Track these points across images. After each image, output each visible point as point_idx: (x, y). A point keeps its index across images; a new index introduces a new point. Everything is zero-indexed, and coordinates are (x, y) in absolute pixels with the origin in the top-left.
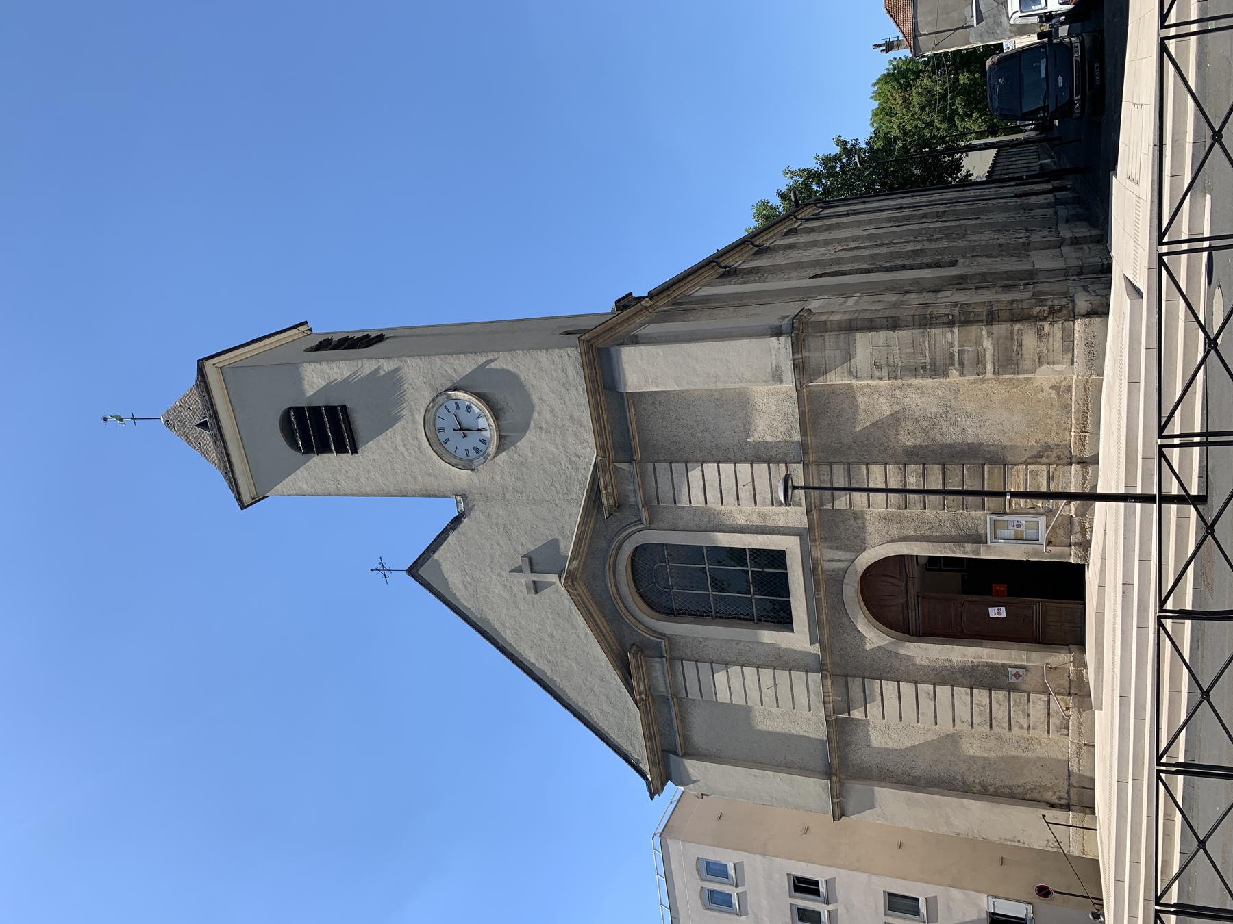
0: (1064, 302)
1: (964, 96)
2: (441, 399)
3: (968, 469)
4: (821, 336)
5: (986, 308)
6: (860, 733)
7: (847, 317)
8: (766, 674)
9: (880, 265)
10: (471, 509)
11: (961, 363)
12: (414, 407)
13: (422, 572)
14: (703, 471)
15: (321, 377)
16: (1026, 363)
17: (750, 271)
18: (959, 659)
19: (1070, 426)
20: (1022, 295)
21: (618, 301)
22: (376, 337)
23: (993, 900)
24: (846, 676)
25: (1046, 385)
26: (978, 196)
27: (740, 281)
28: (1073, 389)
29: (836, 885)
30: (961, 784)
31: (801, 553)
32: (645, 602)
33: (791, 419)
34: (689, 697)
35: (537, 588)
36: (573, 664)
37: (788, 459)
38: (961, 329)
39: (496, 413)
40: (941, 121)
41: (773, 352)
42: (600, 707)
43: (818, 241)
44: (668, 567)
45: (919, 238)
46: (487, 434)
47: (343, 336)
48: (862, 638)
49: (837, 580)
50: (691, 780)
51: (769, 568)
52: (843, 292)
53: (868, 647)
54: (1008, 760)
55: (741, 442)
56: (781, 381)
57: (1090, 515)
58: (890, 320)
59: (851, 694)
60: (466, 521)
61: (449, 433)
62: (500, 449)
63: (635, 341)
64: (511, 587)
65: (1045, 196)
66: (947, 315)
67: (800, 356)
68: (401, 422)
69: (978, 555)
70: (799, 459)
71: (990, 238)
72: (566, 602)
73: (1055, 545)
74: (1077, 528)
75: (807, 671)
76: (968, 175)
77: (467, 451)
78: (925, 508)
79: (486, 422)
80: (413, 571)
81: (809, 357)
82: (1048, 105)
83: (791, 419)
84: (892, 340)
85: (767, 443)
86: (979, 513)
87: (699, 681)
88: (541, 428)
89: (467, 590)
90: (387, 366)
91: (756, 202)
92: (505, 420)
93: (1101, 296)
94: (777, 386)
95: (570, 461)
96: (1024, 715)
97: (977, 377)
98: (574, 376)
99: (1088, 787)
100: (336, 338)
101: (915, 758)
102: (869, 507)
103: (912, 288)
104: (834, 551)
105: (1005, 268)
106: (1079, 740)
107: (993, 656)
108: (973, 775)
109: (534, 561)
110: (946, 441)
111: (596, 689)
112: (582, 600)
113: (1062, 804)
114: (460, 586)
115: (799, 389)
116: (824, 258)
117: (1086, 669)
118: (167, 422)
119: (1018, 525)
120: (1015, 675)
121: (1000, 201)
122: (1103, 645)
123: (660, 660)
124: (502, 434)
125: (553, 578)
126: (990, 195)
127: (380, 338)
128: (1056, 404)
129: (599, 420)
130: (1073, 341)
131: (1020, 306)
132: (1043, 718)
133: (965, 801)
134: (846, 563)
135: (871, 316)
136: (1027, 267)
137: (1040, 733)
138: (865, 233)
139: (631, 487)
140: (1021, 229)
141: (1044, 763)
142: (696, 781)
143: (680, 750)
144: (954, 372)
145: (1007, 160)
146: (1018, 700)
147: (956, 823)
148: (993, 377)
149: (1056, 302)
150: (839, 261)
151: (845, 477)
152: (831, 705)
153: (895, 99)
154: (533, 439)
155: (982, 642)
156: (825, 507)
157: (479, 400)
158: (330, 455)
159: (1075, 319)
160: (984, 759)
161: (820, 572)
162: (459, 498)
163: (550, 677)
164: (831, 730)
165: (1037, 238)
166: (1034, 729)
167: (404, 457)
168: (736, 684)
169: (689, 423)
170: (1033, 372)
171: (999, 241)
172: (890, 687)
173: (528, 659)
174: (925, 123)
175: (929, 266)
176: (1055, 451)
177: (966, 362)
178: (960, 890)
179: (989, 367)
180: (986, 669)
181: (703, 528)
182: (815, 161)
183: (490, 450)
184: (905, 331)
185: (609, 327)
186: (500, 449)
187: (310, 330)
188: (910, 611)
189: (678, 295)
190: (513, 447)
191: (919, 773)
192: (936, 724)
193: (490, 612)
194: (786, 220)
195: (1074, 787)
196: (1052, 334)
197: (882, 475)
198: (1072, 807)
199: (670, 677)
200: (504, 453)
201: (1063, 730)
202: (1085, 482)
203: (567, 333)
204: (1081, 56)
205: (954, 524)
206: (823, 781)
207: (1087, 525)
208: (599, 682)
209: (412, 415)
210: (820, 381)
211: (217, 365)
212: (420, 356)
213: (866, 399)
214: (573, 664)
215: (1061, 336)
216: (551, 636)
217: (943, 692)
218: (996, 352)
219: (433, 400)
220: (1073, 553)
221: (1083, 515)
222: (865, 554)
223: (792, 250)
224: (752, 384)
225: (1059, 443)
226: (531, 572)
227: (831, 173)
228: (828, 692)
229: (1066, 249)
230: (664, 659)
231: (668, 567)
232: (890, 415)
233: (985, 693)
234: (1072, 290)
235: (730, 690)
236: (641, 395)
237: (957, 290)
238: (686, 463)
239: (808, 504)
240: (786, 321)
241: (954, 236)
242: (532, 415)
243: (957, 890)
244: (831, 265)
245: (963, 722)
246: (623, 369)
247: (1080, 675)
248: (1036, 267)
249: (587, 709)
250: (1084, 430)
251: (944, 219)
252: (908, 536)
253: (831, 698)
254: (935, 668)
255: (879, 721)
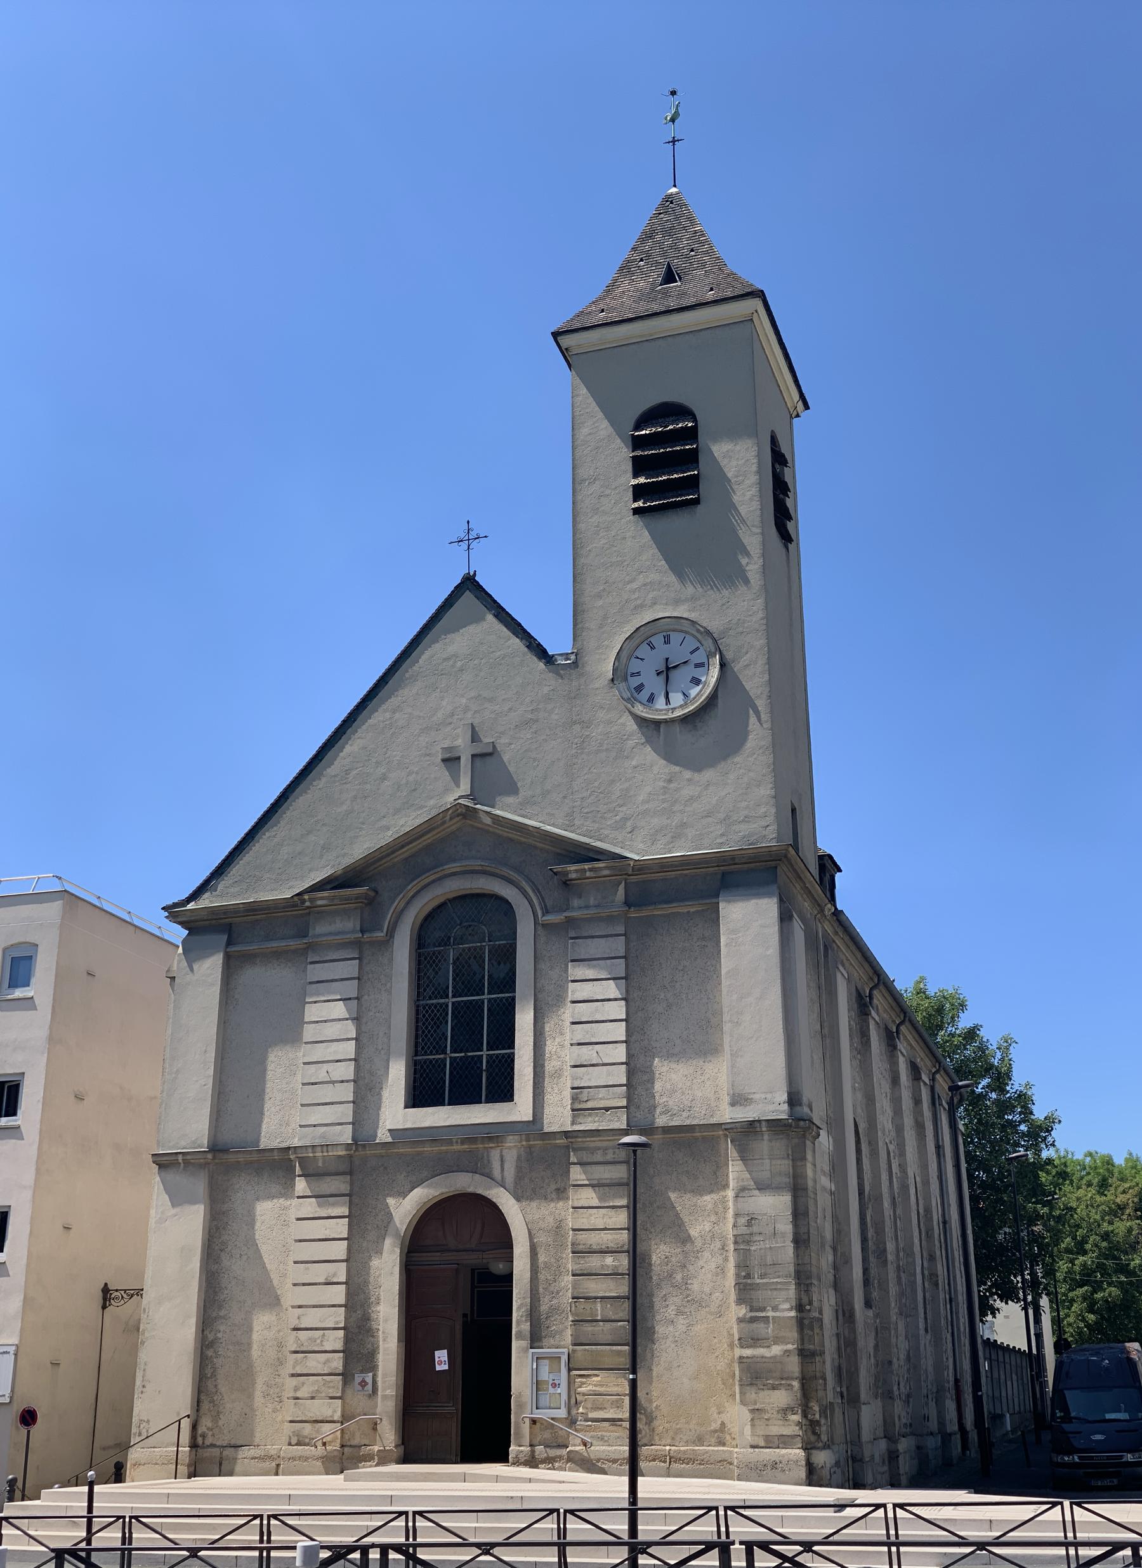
0: (824, 1438)
1: (1122, 1300)
2: (709, 643)
3: (624, 1327)
4: (788, 1155)
5: (818, 1348)
6: (275, 1188)
7: (810, 1183)
8: (347, 1071)
9: (867, 1208)
10: (558, 674)
11: (753, 1320)
12: (698, 603)
13: (468, 597)
14: (616, 1000)
15: (739, 471)
16: (753, 1394)
17: (864, 1035)
18: (381, 1315)
19: (677, 1444)
20: (830, 1391)
21: (830, 857)
22: (787, 531)
23: (12, 1352)
24: (351, 1173)
25: (724, 1417)
26: (959, 1329)
27: (852, 1023)
28: (722, 1448)
29: (14, 1141)
30: (214, 1314)
31: (511, 1122)
32: (434, 910)
33: (685, 1114)
34: (310, 967)
35: (451, 761)
36: (345, 807)
37: (632, 1109)
38: (794, 1321)
39: (687, 720)
40: (1084, 1265)
41: (769, 1096)
42: (285, 843)
43: (902, 1118)
44: (484, 944)
45: (901, 1254)
46: (660, 703)
47: (790, 486)
48: (404, 1195)
49: (478, 1166)
50: (195, 961)
51: (487, 1078)
52: (837, 1169)
53: (391, 1201)
54: (248, 1373)
55: (654, 1050)
56: (733, 1104)
57: (570, 1468)
58: (805, 1237)
59: (328, 1179)
60: (541, 665)
61: (662, 651)
62: (641, 721)
63: (785, 917)
64: (451, 723)
65: (956, 1420)
66: (810, 1303)
67: (764, 1129)
68: (676, 583)
69: (517, 1338)
70: (632, 1124)
71: (900, 1346)
72: (432, 802)
73: (531, 1428)
74: (553, 1453)
75: (353, 1124)
76: (994, 1311)
77: (638, 674)
78: (573, 1275)
79: (678, 705)
80: (469, 583)
81: (763, 1140)
82: (1072, 1422)
83: (685, 1114)
84: (782, 1239)
85: (653, 1083)
86: (569, 1339)
87: (332, 981)
88: (670, 781)
89: (445, 660)
90: (753, 567)
91: (966, 993)
92: (681, 731)
93: (830, 1479)
94: (726, 1099)
95: (626, 819)
96: (313, 1392)
97: (736, 1337)
98: (740, 832)
99: (222, 1468)
100: (789, 503)
101: (244, 1258)
102: (573, 1208)
103: (839, 1254)
104: (514, 1164)
105: (862, 1369)
106: (284, 1458)
107: (388, 1354)
108: (228, 1331)
109: (488, 759)
110: (657, 1300)
111: (312, 838)
112: (438, 827)
113: (196, 1439)
114: (451, 649)
115: (723, 1127)
116: (880, 1133)
117: (376, 1466)
118: (669, 199)
119: (554, 1385)
120: (363, 1381)
121: (951, 1360)
122: (426, 1481)
123: (358, 928)
124: (662, 726)
125: (465, 787)
126: (960, 1346)
127: (786, 537)
128: (703, 1429)
129: (682, 865)
130: (778, 1448)
131: (819, 1387)
132: (310, 1416)
133: (193, 1321)
134: (500, 1178)
135: (811, 1214)
136: (863, 1396)
137: (290, 1410)
138: (911, 1181)
139: (592, 902)
140: (910, 1389)
141: (247, 1417)
142: (192, 970)
143: (233, 949)
144: (743, 1311)
145: (1014, 1369)
146: (331, 1384)
147: (161, 1309)
148: (737, 1355)
149: (824, 1428)
150: (874, 1153)
151: (611, 1179)
152: (311, 1155)
153: (1124, 1192)
154: (656, 769)
155: (402, 1341)
156: (572, 1154)
157: (707, 697)
158: (630, 474)
159: (805, 1449)
160: (250, 1345)
161: (487, 1146)
162: (573, 657)
163: (324, 773)
164: (276, 1153)
165: (898, 1408)
166: (295, 1404)
167: (630, 582)
168: (332, 1030)
169: (678, 984)
170: (743, 1403)
171: (895, 1360)
172: (341, 1228)
173: (350, 742)
174: (1082, 1240)
175: (866, 1271)
176: (646, 1428)
177: (755, 1325)
178: (21, 1309)
179: (748, 1352)
180: (369, 1346)
181: (540, 996)
182: (1023, 1083)
183: (640, 708)
184: (792, 1255)
185: (802, 876)
186: (641, 721)
187: (798, 416)
188: (439, 1254)
189: (836, 944)
190: (643, 740)
191: (226, 1262)
192: (295, 1285)
193: (414, 691)
194: (932, 1058)
195: (221, 1453)
196: (788, 1423)
197: (615, 1225)
198: (194, 1450)
199: (336, 942)
200: (635, 727)
201: (296, 1438)
202: (610, 1462)
203: (793, 810)
204: (1128, 1462)
205: (554, 1310)
206: (206, 1142)
207: (557, 1465)
208: (322, 842)
209: (686, 600)
210: (732, 1152)
211: (755, 314)
212: (767, 618)
213: (710, 1206)
214: (345, 807)
215: (784, 1433)
216: (384, 778)
217: (338, 1294)
218: (766, 1360)
219: (708, 633)
220: (522, 1448)
221: (569, 1460)
222: (512, 1201)
223: (889, 1081)
224: (730, 1068)
225: (656, 1432)
226: (473, 756)
227: (1004, 1106)
228: (327, 1152)
229: (883, 1445)
230: (361, 935)
231: (484, 944)
232: (689, 1236)
233: (339, 1345)
234: (836, 1448)
235: (321, 1022)
236: (716, 921)
237: (837, 1311)
238: (626, 978)
239: (575, 1134)
240: (806, 1110)
241: (904, 1301)
242: (688, 769)
243: (21, 1303)
244: (870, 1143)
245: (299, 1318)
246: (748, 900)
247: (368, 1458)
248: (863, 1407)
249: (282, 823)
250: (672, 1460)
251: (926, 1285)
252: (537, 1254)
253: (321, 1154)
254: (366, 1283)
255: (293, 1214)
